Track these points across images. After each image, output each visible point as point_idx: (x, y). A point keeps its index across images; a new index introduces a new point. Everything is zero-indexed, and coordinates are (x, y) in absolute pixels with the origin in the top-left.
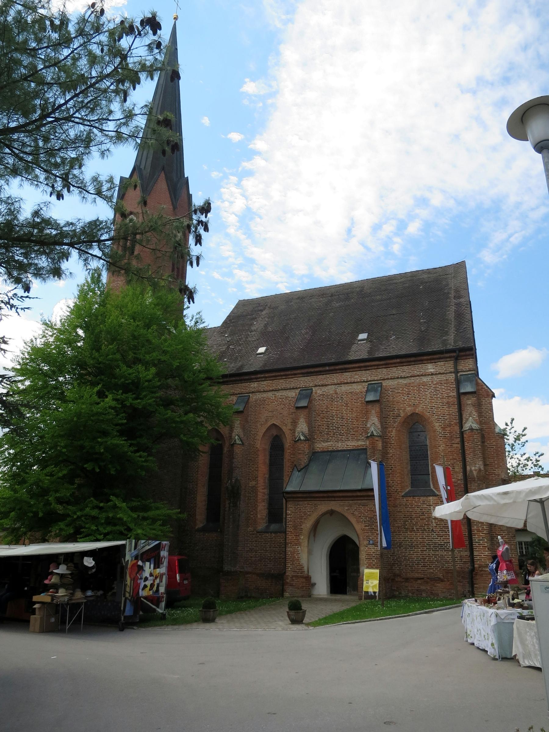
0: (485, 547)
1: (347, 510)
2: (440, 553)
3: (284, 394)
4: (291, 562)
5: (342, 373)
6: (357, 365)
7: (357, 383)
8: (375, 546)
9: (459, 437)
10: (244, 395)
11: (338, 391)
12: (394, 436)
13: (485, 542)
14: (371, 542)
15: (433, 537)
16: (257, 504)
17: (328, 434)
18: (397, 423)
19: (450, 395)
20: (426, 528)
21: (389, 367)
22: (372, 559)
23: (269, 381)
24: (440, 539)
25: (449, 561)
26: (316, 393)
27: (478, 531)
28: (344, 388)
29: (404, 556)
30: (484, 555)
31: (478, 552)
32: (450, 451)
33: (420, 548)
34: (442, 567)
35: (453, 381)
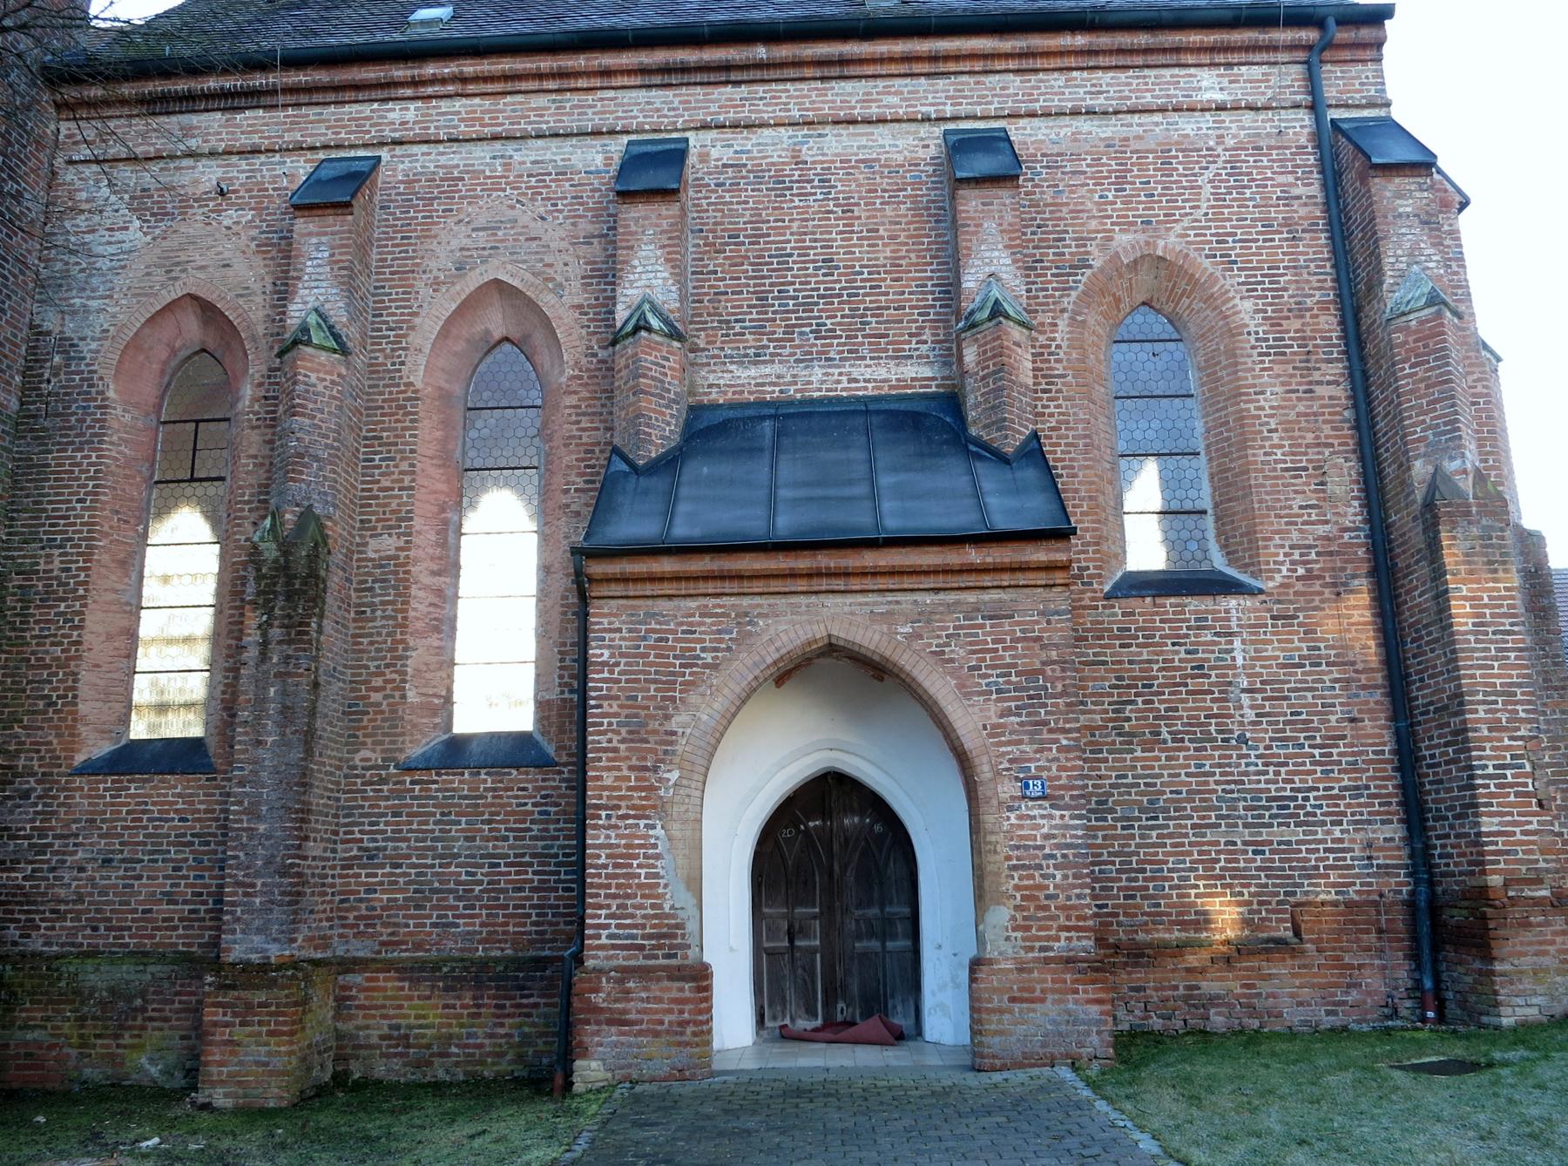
0: (1527, 794)
1: (909, 637)
2: (1277, 833)
3: (548, 156)
4: (614, 904)
5: (823, 79)
6: (899, 47)
7: (896, 125)
8: (1052, 806)
9: (1337, 360)
10: (352, 154)
11: (807, 154)
12: (1065, 344)
13: (1526, 775)
14: (1035, 789)
15: (1243, 768)
16: (403, 641)
17: (759, 330)
18: (1074, 294)
19: (1296, 192)
20: (1213, 728)
21: (1036, 71)
22: (1040, 867)
23: (477, 101)
24: (1277, 773)
25: (1317, 868)
26: (704, 158)
27: (1495, 727)
28: (836, 143)
29: (1116, 854)
30: (1524, 833)
31: (1496, 820)
32: (1307, 415)
33: (1191, 818)
34: (1286, 893)
35: (1303, 141)
